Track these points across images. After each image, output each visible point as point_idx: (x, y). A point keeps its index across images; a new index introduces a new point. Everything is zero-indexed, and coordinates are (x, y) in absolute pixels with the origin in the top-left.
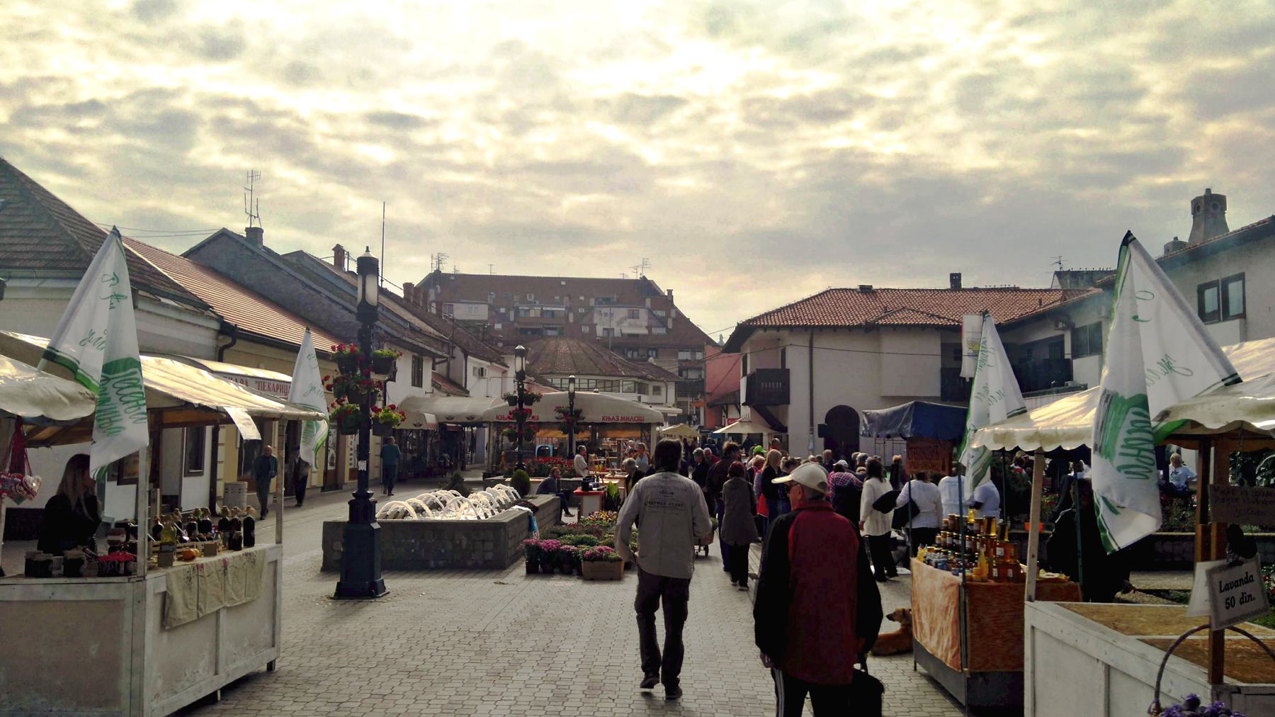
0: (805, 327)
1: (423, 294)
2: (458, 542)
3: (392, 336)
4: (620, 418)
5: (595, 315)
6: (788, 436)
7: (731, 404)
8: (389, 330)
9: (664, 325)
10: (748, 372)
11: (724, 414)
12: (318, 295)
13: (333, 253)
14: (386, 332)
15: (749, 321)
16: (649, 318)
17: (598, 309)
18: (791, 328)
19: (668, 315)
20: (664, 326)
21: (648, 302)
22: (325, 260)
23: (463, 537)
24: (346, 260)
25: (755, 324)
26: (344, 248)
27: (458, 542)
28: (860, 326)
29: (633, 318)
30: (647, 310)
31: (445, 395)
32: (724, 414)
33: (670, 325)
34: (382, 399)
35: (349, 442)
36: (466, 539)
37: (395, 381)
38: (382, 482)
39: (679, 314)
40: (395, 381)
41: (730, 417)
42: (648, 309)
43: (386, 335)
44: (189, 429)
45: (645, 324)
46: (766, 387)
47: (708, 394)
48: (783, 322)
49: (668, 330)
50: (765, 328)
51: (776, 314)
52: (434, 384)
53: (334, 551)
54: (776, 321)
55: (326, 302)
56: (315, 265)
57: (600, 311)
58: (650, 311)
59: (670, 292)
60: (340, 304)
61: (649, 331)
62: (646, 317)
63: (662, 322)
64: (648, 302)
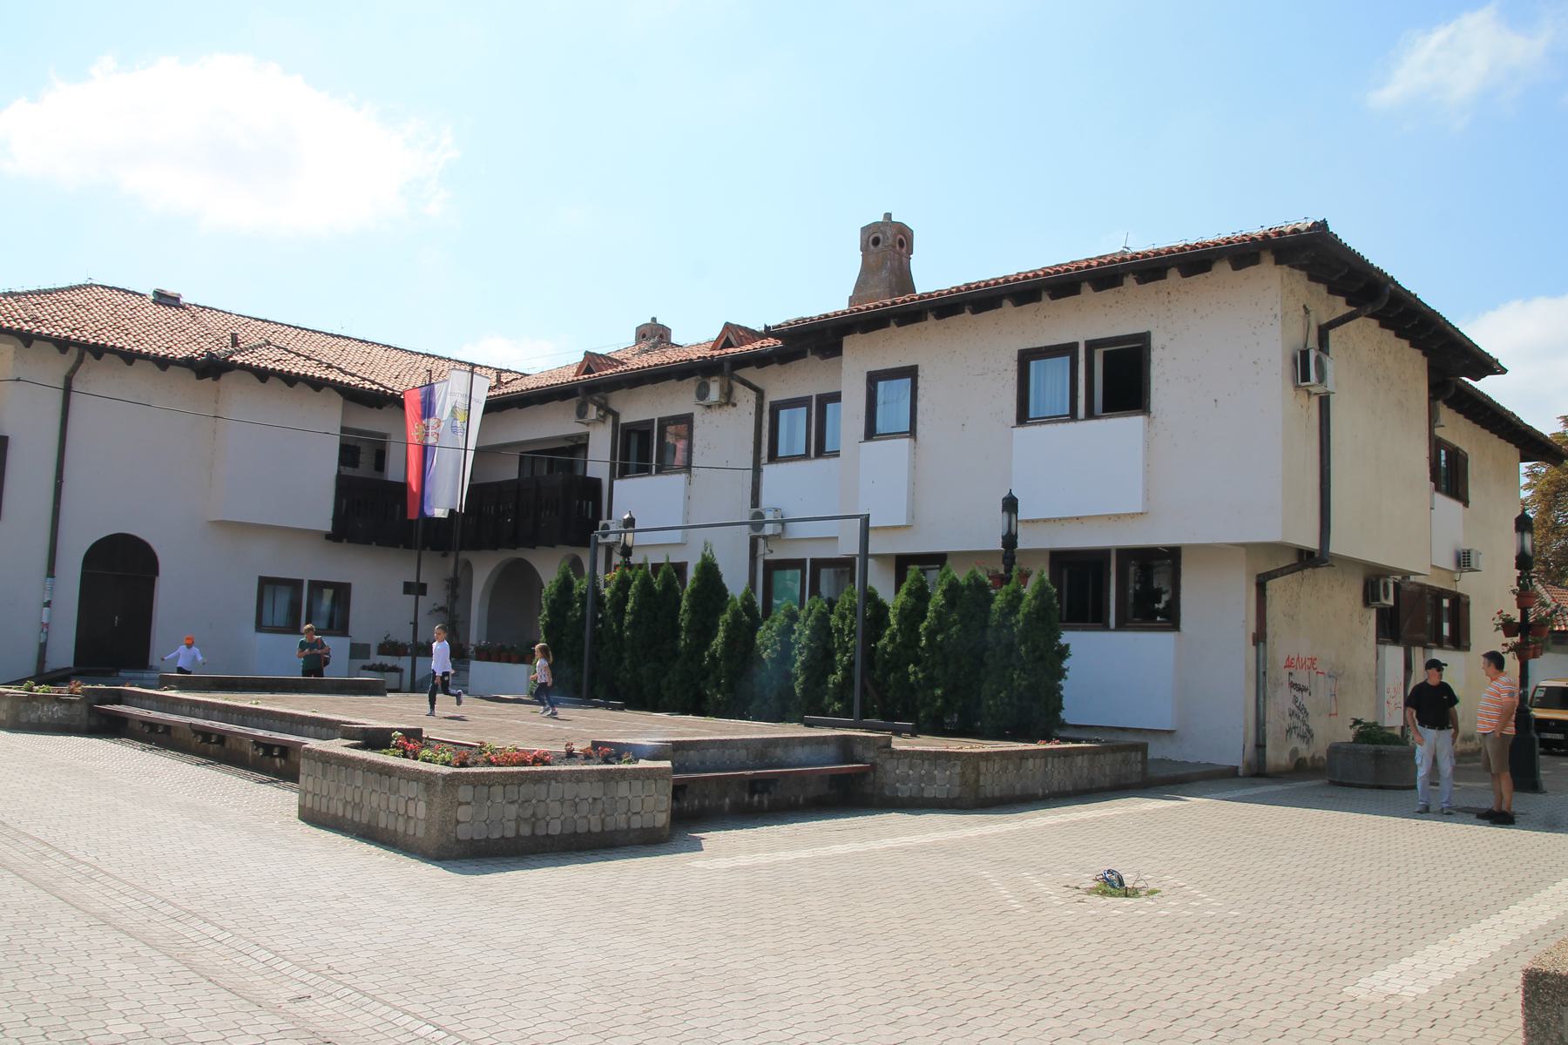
0: (63, 344)
28: (188, 363)
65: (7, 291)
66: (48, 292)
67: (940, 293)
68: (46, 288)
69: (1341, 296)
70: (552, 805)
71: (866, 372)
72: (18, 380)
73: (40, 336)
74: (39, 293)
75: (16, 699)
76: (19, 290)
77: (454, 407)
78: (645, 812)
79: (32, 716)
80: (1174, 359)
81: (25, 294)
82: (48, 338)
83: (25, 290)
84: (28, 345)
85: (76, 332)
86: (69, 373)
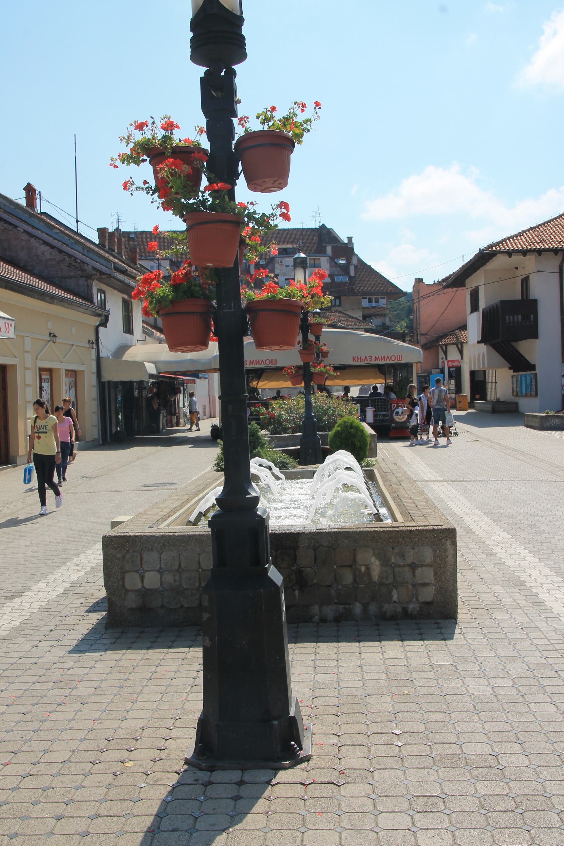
1: (118, 239)
2: (363, 569)
3: (102, 273)
4: (373, 358)
5: (277, 266)
6: (536, 375)
7: (450, 344)
8: (98, 266)
9: (347, 272)
10: (482, 305)
11: (441, 355)
12: (15, 230)
13: (24, 193)
14: (94, 268)
15: (491, 246)
16: (331, 267)
17: (279, 259)
18: (539, 252)
19: (349, 262)
20: (346, 275)
21: (329, 250)
22: (16, 201)
23: (373, 559)
24: (38, 201)
25: (494, 249)
26: (35, 187)
27: (363, 569)
29: (315, 267)
30: (329, 258)
31: (158, 342)
32: (441, 355)
33: (352, 273)
34: (95, 347)
35: (298, 340)
36: (378, 563)
37: (106, 327)
38: (101, 443)
39: (360, 261)
40: (106, 327)
41: (449, 359)
42: (330, 257)
43: (94, 272)
44: (208, 535)
45: (327, 273)
46: (511, 320)
47: (423, 335)
48: (530, 245)
49: (350, 278)
50: (509, 253)
51: (519, 238)
52: (145, 332)
53: (127, 591)
54: (520, 244)
55: (25, 237)
56: (7, 204)
57: (281, 262)
58: (332, 259)
59: (350, 239)
60: (40, 239)
61: (331, 280)
62: (328, 266)
63: (345, 269)
64: (329, 250)
65: (529, 228)
66: (549, 222)
67: (471, 260)
68: (547, 220)
69: (331, 280)
70: (310, 793)
71: (455, 526)
72: (538, 271)
73: (545, 250)
74: (544, 224)
75: (542, 418)
76: (535, 225)
77: (479, 354)
78: (412, 816)
79: (548, 424)
80: (443, 9)
81: (538, 227)
82: (548, 250)
83: (537, 224)
84: (540, 255)
85: (561, 243)
86: (560, 264)
